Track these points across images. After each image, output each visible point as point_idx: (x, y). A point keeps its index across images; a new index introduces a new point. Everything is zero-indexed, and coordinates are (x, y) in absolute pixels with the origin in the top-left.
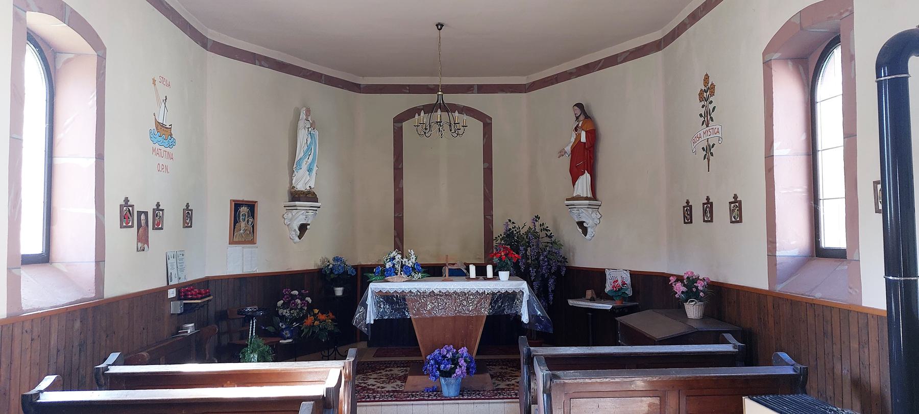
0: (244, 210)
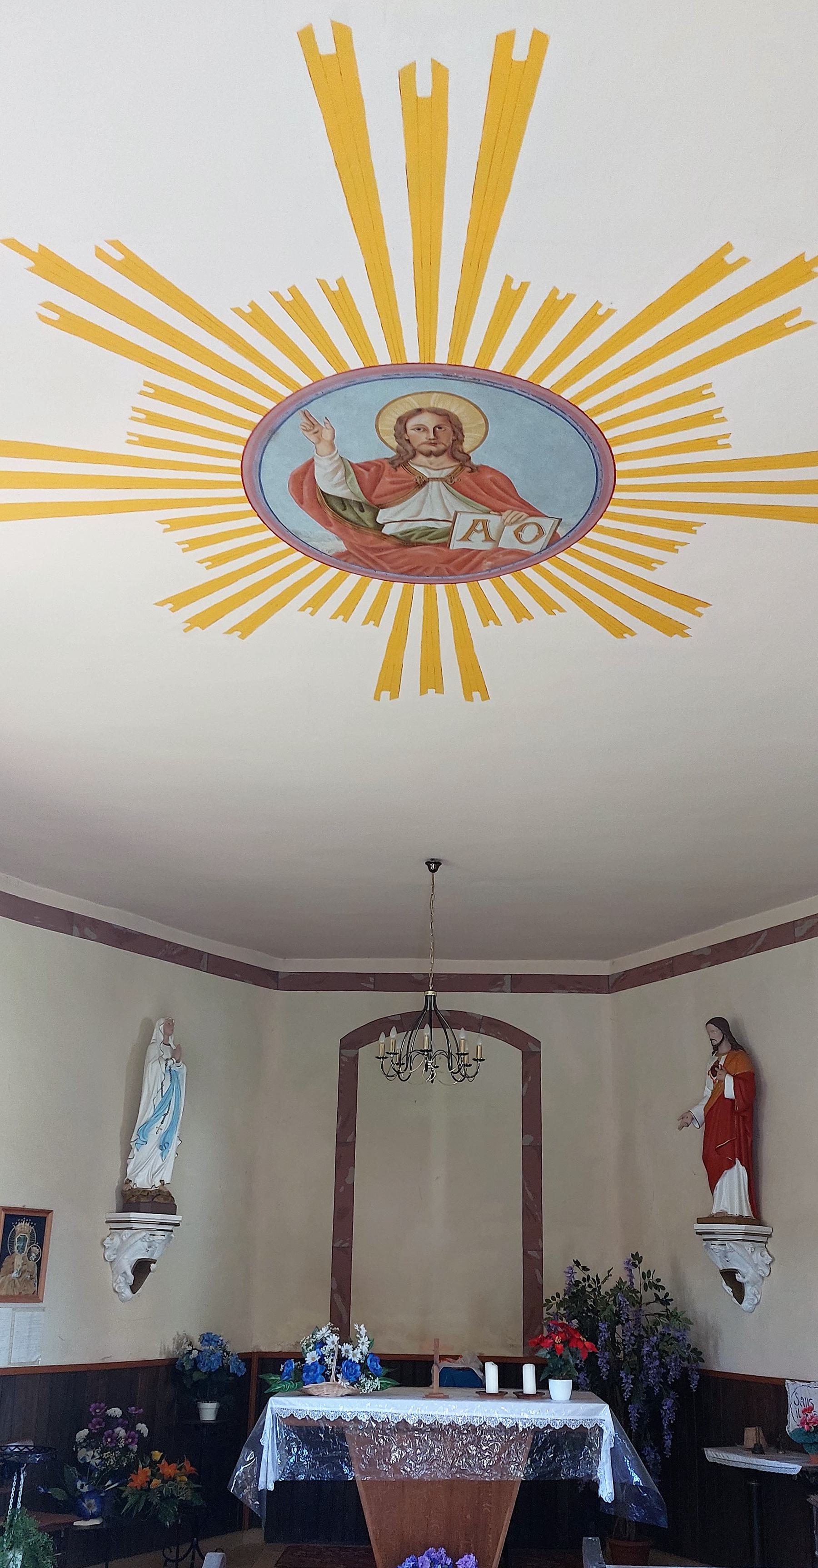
0: (23, 1228)
